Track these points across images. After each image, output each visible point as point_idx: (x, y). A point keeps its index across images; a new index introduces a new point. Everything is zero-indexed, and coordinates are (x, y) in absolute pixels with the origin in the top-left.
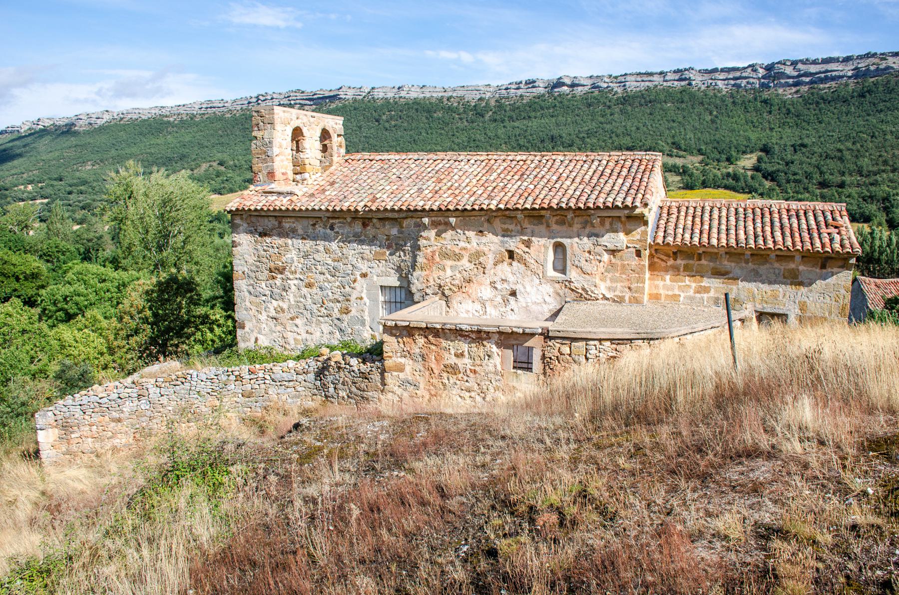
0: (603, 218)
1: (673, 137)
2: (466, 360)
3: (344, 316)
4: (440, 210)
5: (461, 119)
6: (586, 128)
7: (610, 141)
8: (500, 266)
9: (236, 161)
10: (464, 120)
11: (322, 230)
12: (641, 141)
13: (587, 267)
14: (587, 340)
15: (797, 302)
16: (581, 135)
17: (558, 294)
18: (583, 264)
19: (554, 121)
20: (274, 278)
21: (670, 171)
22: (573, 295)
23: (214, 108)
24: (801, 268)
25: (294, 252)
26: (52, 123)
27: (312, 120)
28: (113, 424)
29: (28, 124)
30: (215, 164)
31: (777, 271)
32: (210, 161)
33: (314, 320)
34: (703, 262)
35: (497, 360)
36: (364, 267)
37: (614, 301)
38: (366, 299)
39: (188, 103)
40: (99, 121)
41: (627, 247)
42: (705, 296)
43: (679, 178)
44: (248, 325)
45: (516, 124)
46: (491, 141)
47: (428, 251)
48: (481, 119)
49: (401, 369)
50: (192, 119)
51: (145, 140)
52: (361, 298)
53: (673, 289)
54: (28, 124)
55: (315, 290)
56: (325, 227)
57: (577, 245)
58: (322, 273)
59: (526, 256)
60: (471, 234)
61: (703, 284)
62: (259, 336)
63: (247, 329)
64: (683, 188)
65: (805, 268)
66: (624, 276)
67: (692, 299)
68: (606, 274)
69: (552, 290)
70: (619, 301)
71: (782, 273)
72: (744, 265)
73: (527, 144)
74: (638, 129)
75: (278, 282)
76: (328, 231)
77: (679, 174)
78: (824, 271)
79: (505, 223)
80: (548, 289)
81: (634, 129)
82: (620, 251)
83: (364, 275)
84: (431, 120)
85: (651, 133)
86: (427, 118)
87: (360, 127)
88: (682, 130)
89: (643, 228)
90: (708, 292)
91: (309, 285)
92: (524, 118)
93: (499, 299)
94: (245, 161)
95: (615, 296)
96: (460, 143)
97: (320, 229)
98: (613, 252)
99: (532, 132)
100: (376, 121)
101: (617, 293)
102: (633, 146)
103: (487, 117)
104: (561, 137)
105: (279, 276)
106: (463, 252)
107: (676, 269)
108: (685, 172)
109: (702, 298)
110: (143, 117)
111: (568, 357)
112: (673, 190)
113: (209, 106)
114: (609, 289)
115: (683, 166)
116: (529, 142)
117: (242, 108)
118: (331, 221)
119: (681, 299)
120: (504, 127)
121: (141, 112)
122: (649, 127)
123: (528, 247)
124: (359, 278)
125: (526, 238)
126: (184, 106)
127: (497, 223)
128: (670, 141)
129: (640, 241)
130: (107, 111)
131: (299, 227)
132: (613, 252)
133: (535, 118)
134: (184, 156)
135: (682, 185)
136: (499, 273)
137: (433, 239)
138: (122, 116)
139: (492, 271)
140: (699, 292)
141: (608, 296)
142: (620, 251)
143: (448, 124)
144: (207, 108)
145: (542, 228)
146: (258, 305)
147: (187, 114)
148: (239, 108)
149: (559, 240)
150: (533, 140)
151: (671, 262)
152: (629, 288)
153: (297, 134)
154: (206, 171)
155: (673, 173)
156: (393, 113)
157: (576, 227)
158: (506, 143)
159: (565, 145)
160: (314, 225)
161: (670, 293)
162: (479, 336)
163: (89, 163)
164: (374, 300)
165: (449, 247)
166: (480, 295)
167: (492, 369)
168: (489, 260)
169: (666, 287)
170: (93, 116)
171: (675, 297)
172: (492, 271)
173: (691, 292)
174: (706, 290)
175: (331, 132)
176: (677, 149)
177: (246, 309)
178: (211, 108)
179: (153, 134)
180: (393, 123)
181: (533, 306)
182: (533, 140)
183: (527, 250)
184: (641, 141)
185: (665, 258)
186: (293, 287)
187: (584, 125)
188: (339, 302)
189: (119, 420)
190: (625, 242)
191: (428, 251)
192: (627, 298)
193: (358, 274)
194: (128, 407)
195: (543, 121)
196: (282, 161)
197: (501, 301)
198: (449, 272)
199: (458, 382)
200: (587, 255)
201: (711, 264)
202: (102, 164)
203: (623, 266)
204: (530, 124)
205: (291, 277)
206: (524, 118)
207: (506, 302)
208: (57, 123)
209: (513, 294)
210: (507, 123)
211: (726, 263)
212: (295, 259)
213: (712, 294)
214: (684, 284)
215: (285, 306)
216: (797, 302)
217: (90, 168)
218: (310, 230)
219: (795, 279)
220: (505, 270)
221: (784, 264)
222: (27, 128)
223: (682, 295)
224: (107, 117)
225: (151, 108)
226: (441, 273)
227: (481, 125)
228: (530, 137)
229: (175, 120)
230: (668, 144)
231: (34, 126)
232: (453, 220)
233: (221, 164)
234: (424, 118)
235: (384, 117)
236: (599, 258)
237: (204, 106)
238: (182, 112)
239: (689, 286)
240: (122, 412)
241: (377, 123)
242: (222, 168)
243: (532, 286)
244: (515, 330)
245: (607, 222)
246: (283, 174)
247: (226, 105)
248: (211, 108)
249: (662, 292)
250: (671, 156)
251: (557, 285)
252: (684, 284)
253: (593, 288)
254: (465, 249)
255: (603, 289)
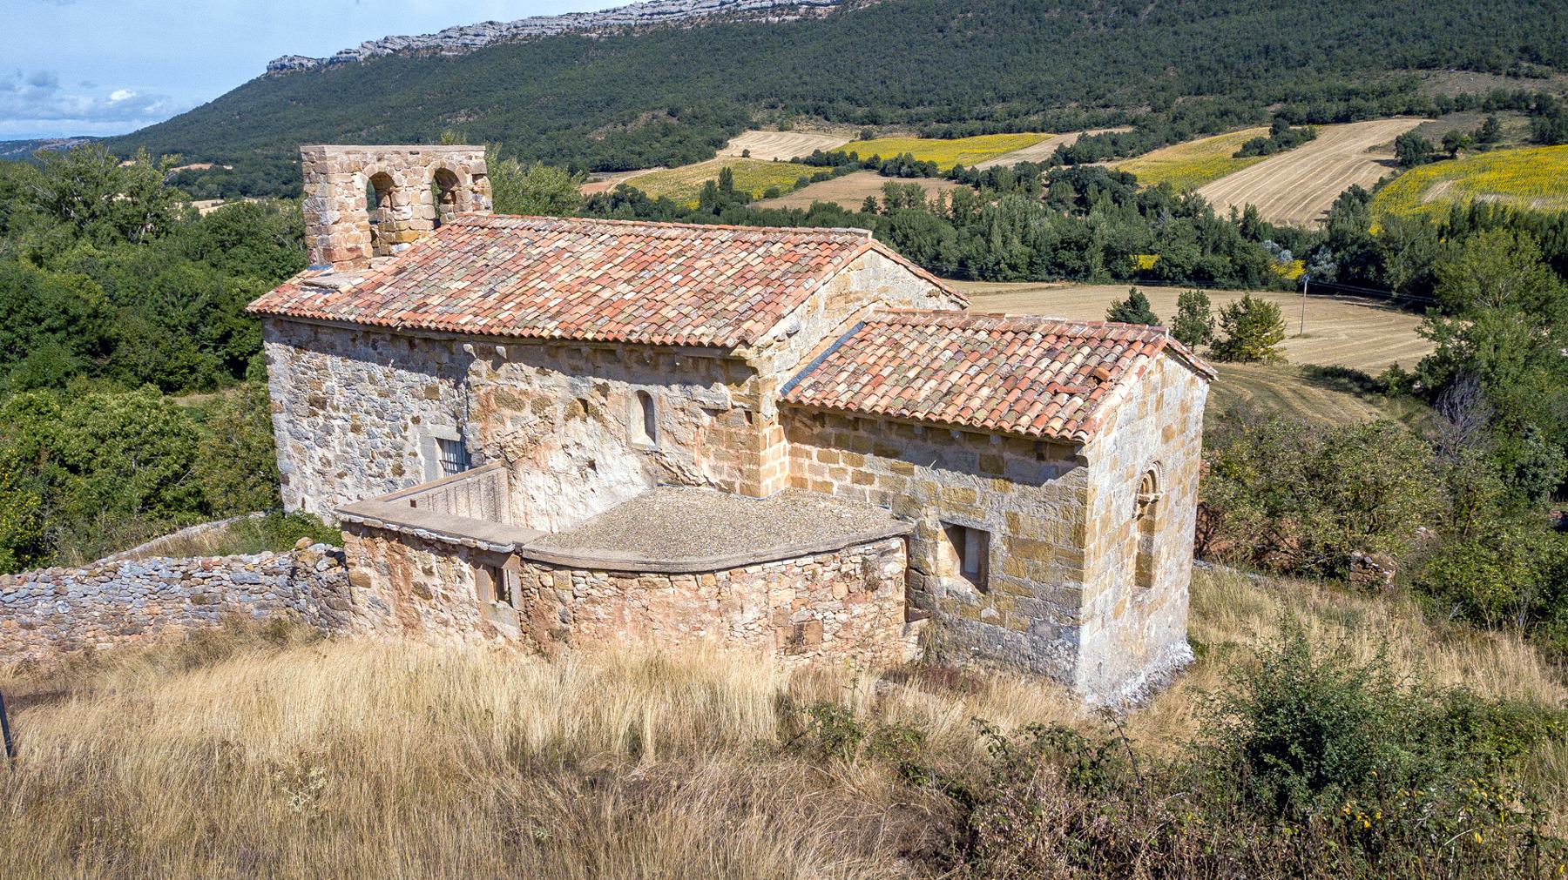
0: (696, 360)
1: (1526, 36)
2: (437, 581)
3: (397, 477)
4: (482, 333)
5: (1094, 22)
6: (1339, 29)
7: (1385, 52)
8: (571, 423)
9: (696, 108)
10: (1100, 24)
11: (363, 348)
12: (1451, 49)
13: (682, 433)
14: (573, 568)
15: (1003, 511)
16: (1326, 44)
17: (647, 471)
18: (677, 428)
19: (1274, 17)
20: (315, 414)
21: (1509, 107)
22: (666, 474)
23: (664, 13)
24: (1007, 455)
25: (335, 379)
26: (406, 44)
27: (411, 158)
28: (24, 632)
29: (370, 46)
30: (662, 114)
31: (970, 458)
32: (654, 109)
33: (365, 480)
34: (862, 433)
35: (470, 584)
36: (414, 407)
37: (721, 489)
38: (420, 456)
39: (621, 5)
40: (478, 41)
41: (734, 407)
42: (867, 488)
43: (1526, 122)
44: (293, 480)
45: (1196, 27)
46: (1146, 62)
47: (481, 393)
48: (1132, 20)
49: (366, 583)
50: (627, 34)
51: (551, 72)
52: (415, 455)
53: (822, 474)
54: (370, 46)
55: (363, 437)
56: (366, 345)
57: (667, 395)
58: (367, 413)
59: (602, 410)
60: (531, 371)
61: (863, 469)
62: (306, 497)
63: (292, 485)
64: (1534, 143)
65: (1013, 456)
66: (732, 451)
67: (849, 491)
68: (708, 446)
69: (639, 465)
70: (727, 489)
71: (977, 462)
72: (920, 442)
73: (1215, 66)
74: (1449, 24)
75: (321, 420)
76: (371, 350)
77: (1530, 113)
78: (1043, 463)
79: (572, 358)
80: (633, 462)
81: (1440, 24)
82: (724, 411)
83: (416, 420)
84: (1037, 25)
85: (1477, 30)
86: (1031, 23)
87: (910, 44)
88: (1548, 20)
89: (752, 378)
90: (871, 483)
91: (356, 429)
92: (1215, 14)
93: (574, 472)
94: (712, 108)
95: (722, 481)
96: (1087, 68)
97: (361, 347)
98: (715, 412)
99: (1228, 41)
100: (941, 31)
101: (725, 477)
102: (1434, 60)
103: (1144, 15)
104: (1284, 49)
105: (321, 412)
106: (523, 398)
107: (824, 442)
108: (1540, 110)
109: (863, 492)
110: (549, 32)
111: (551, 591)
112: (1509, 147)
113: (656, 10)
114: (714, 469)
115: (1539, 97)
116: (1219, 61)
117: (710, 13)
118: (373, 337)
119: (835, 490)
120: (1175, 33)
121: (544, 23)
122: (1475, 19)
123: (605, 396)
124: (410, 423)
125: (600, 381)
126: (614, 11)
127: (563, 357)
128: (1516, 44)
129: (750, 397)
130: (491, 23)
131: (337, 340)
132: (715, 412)
133: (1237, 12)
134: (613, 100)
135: (1529, 136)
136: (571, 432)
137: (484, 375)
138: (514, 31)
139: (563, 429)
140: (858, 482)
141: (713, 480)
142: (724, 411)
143: (1070, 32)
144: (652, 15)
145: (620, 368)
146: (300, 451)
147: (620, 25)
148: (704, 13)
149: (643, 387)
150: (1228, 57)
151: (817, 430)
152: (740, 471)
153: (380, 187)
154: (647, 125)
155: (1515, 112)
156: (969, 15)
157: (663, 370)
158: (1175, 63)
159: (1292, 63)
160: (354, 340)
161: (819, 479)
162: (446, 549)
163: (462, 112)
164: (430, 457)
165: (506, 389)
166: (550, 463)
167: (465, 596)
168: (559, 411)
169: (812, 469)
170: (468, 31)
171: (826, 486)
172: (563, 429)
173: (848, 481)
174: (868, 479)
175: (457, 171)
176: (1532, 61)
177: (289, 457)
178: (659, 13)
179: (564, 62)
180: (969, 33)
181: (618, 487)
182: (1228, 57)
183: (603, 400)
184: (1451, 49)
185: (808, 422)
186: (337, 430)
187: (1335, 22)
188: (391, 457)
189: (30, 627)
190: (729, 399)
191: (481, 393)
192: (737, 486)
193: (409, 417)
194: (41, 608)
195: (1251, 18)
196: (347, 230)
197: (578, 476)
198: (509, 427)
199: (431, 611)
200: (681, 414)
201: (872, 437)
202: (482, 114)
203: (730, 435)
204: (1225, 26)
205: (334, 414)
206: (1215, 14)
207: (585, 477)
208: (414, 45)
209: (592, 465)
210: (1182, 26)
211: (894, 436)
212: (337, 388)
213: (876, 486)
214: (836, 466)
215: (331, 457)
216: (1003, 511)
217: (462, 120)
218: (351, 348)
219: (993, 469)
220: (579, 429)
221: (981, 446)
222: (368, 53)
223: (836, 483)
224: (490, 33)
225: (561, 17)
226: (500, 427)
227: (1130, 30)
228: (1221, 51)
229: (601, 35)
230: (1511, 51)
231: (379, 51)
232: (501, 349)
233: (672, 114)
234: (1025, 23)
235: (954, 24)
236: (695, 420)
237: (648, 11)
238: (612, 22)
239: (844, 470)
240: (34, 615)
241: (940, 35)
242: (674, 121)
243: (614, 457)
244: (479, 544)
245: (702, 366)
246: (350, 250)
247: (683, 8)
248: (659, 13)
249: (807, 475)
250: (1516, 76)
251: (646, 458)
252: (836, 466)
253: (691, 467)
254: (525, 393)
255: (704, 469)
